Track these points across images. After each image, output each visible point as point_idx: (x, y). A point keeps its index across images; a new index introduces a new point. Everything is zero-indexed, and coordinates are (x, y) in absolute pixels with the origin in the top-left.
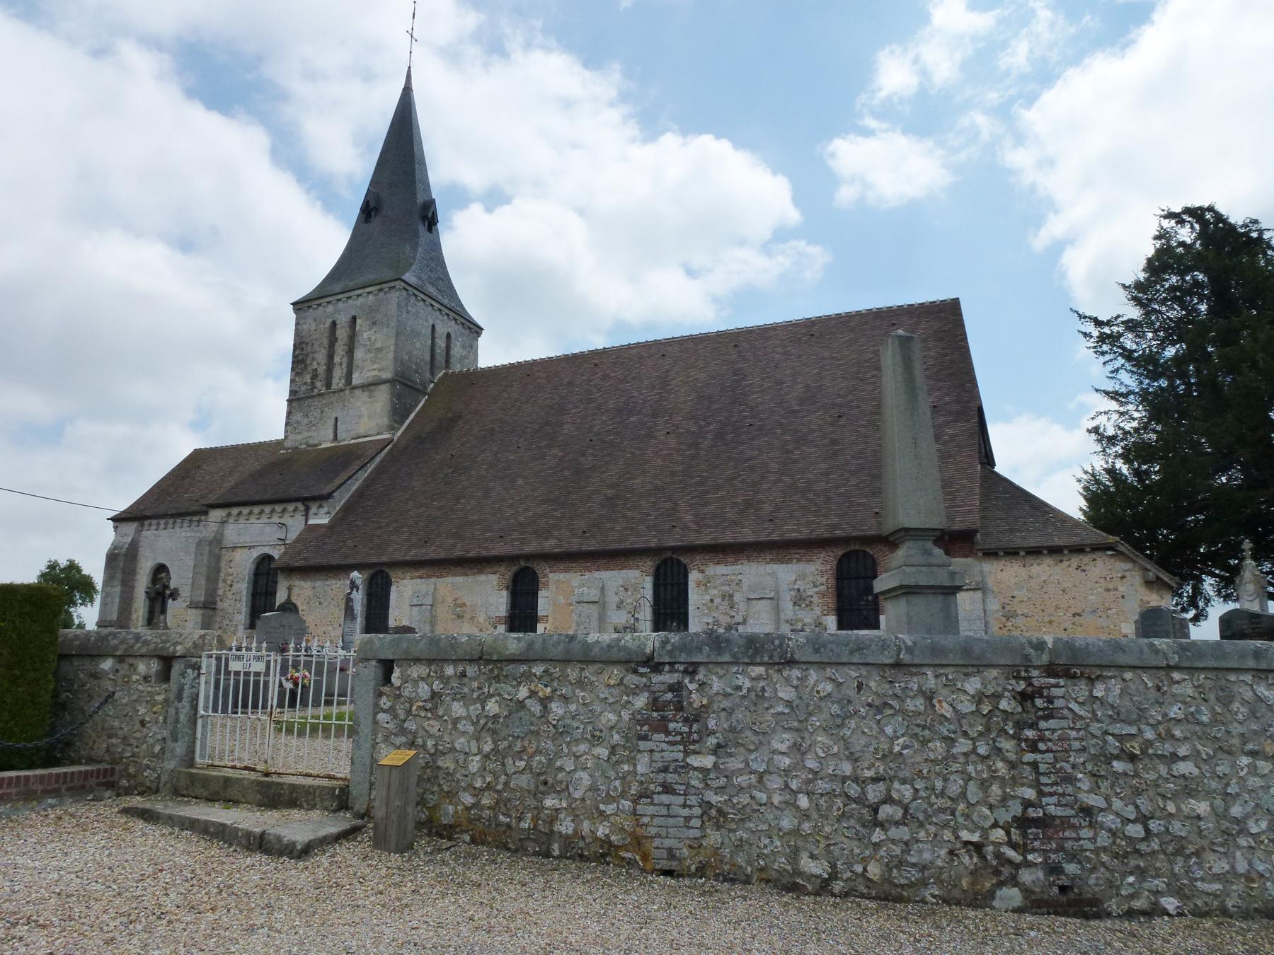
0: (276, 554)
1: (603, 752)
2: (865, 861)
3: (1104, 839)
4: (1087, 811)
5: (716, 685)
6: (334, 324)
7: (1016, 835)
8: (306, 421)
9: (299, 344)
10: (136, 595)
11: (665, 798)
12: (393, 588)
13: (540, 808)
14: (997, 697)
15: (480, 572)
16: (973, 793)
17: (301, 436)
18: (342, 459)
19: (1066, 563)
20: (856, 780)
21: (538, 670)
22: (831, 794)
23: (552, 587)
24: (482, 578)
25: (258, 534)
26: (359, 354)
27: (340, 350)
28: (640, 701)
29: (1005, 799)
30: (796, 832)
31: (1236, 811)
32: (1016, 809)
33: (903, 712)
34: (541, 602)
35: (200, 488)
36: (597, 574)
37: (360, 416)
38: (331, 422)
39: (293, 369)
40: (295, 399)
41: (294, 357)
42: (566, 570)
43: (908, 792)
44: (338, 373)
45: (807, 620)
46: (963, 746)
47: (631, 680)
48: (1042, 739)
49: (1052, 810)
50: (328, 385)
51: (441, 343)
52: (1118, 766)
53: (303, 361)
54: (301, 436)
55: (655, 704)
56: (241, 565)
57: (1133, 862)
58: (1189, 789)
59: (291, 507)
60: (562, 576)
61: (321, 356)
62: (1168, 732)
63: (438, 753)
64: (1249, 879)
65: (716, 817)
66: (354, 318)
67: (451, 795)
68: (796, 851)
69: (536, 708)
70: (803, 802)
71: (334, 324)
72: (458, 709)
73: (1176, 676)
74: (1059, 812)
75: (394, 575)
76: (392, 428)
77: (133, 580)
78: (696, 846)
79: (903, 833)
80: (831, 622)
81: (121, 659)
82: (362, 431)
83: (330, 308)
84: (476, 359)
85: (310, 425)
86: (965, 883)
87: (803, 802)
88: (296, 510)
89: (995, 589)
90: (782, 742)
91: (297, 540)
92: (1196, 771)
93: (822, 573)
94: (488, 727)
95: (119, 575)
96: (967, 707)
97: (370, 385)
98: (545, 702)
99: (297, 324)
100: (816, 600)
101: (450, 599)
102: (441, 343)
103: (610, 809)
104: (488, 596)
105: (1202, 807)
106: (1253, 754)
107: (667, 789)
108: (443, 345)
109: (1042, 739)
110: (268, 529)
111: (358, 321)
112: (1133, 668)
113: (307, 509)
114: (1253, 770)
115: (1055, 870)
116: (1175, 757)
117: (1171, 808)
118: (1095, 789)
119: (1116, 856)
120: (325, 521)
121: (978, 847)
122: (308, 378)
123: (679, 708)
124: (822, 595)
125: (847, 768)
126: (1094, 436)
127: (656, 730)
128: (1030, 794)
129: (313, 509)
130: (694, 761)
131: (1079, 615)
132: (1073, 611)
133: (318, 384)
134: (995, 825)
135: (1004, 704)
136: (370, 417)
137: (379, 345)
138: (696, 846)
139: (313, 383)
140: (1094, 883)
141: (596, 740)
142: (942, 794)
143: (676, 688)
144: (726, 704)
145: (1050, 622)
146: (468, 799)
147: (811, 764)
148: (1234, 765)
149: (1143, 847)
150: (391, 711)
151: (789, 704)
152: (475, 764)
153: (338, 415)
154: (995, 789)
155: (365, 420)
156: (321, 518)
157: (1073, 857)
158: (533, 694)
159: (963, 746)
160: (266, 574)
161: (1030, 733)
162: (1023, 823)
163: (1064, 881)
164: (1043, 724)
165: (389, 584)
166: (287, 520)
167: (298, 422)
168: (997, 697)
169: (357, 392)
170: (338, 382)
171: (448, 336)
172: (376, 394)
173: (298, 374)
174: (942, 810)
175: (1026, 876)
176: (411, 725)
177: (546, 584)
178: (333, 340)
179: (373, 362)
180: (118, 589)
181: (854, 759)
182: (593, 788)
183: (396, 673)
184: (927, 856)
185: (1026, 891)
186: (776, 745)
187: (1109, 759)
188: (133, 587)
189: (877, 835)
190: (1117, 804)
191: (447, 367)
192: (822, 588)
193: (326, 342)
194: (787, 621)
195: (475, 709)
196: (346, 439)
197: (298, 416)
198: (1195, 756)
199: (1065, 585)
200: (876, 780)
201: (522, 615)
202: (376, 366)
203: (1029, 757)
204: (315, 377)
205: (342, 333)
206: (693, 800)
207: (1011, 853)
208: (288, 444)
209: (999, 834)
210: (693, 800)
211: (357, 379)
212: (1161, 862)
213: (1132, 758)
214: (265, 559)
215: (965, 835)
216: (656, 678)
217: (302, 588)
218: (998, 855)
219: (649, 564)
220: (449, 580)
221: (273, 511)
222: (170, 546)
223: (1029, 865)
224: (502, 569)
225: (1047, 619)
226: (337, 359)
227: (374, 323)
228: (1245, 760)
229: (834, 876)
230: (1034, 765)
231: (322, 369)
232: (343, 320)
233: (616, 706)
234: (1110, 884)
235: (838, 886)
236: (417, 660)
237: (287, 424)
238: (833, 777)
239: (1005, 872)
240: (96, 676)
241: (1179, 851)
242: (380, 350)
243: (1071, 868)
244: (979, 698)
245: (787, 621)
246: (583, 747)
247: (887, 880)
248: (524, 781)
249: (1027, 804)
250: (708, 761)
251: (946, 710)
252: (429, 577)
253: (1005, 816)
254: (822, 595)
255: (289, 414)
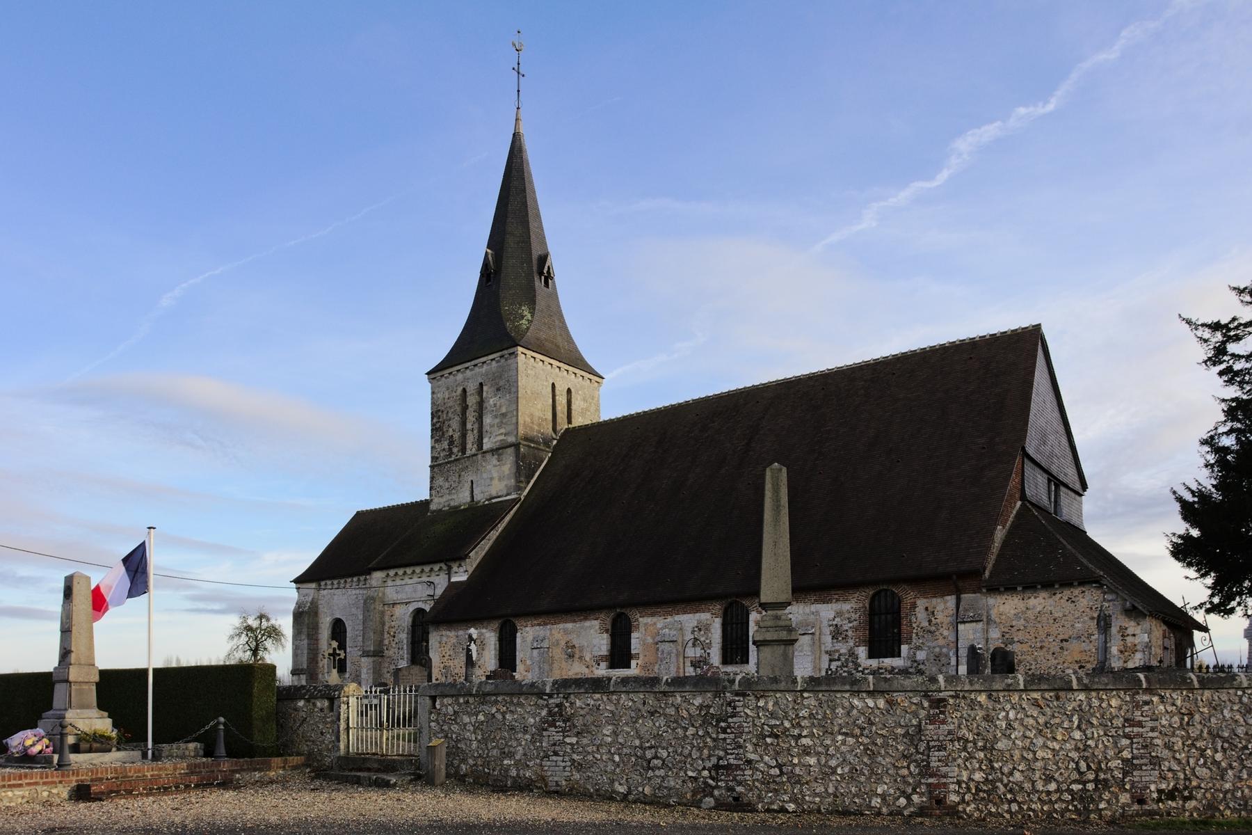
0: (427, 608)
1: (528, 737)
2: (644, 786)
3: (759, 775)
4: (749, 762)
5: (578, 703)
6: (464, 391)
7: (713, 773)
8: (447, 485)
9: (438, 416)
10: (320, 636)
11: (554, 758)
12: (518, 635)
13: (502, 765)
14: (709, 707)
15: (586, 619)
16: (695, 754)
17: (445, 499)
18: (478, 517)
19: (1059, 596)
20: (641, 748)
21: (500, 699)
22: (630, 755)
23: (642, 629)
24: (587, 624)
25: (411, 590)
26: (487, 420)
27: (471, 416)
28: (544, 713)
29: (710, 756)
30: (613, 772)
31: (833, 763)
32: (714, 760)
33: (665, 715)
34: (633, 641)
35: (367, 546)
36: (677, 618)
37: (492, 479)
38: (468, 485)
39: (432, 437)
40: (437, 466)
41: (433, 425)
42: (652, 615)
43: (665, 755)
44: (471, 438)
45: (843, 651)
46: (691, 731)
47: (541, 702)
48: (729, 727)
49: (732, 761)
50: (463, 450)
51: (562, 400)
52: (769, 740)
53: (440, 429)
54: (445, 499)
55: (550, 713)
56: (403, 616)
57: (772, 786)
58: (806, 751)
59: (436, 567)
60: (649, 620)
61: (455, 424)
62: (798, 724)
63: (458, 741)
64: (835, 796)
65: (579, 766)
66: (481, 384)
67: (464, 761)
68: (613, 781)
69: (499, 716)
70: (617, 758)
71: (464, 391)
72: (466, 719)
73: (806, 695)
74: (735, 762)
75: (519, 624)
76: (519, 489)
77: (317, 633)
78: (568, 780)
79: (662, 773)
80: (862, 652)
81: (308, 701)
82: (494, 494)
83: (460, 377)
84: (598, 410)
85: (450, 489)
86: (688, 796)
87: (617, 758)
88: (441, 569)
89: (998, 620)
90: (607, 730)
91: (442, 596)
92: (811, 743)
93: (856, 611)
94: (477, 727)
95: (305, 630)
96: (693, 711)
97: (498, 449)
98: (504, 714)
99: (433, 393)
100: (850, 633)
101: (563, 643)
102: (562, 400)
103: (531, 764)
104: (592, 637)
105: (812, 761)
106: (846, 734)
107: (556, 754)
108: (565, 402)
109: (729, 727)
110: (420, 586)
111: (485, 388)
112: (781, 691)
113: (450, 568)
114: (844, 742)
115: (731, 789)
116: (800, 736)
117: (796, 761)
118: (755, 751)
119: (763, 783)
120: (464, 578)
121: (695, 779)
122: (445, 445)
123: (561, 715)
124: (856, 629)
125: (637, 742)
126: (1207, 448)
127: (550, 726)
128: (721, 753)
129: (455, 568)
130: (568, 740)
131: (1066, 641)
132: (1061, 637)
133: (455, 450)
134: (704, 768)
135: (712, 711)
136: (500, 480)
137: (504, 410)
138: (568, 780)
139: (450, 449)
140: (751, 796)
141: (525, 732)
142: (681, 754)
143: (560, 705)
144: (582, 712)
145: (1041, 648)
146: (471, 762)
147: (621, 740)
148: (834, 740)
149: (778, 779)
150: (436, 721)
151: (612, 712)
152: (475, 745)
153: (474, 478)
154: (706, 752)
155: (496, 482)
156: (460, 576)
157: (740, 783)
158: (498, 710)
159: (691, 731)
160: (422, 625)
161: (723, 724)
162: (717, 767)
163: (735, 795)
164: (730, 720)
165: (516, 631)
166: (433, 578)
167: (441, 487)
168: (709, 707)
169: (488, 456)
170: (471, 448)
171: (569, 391)
172: (504, 457)
173: (436, 441)
174: (680, 762)
175: (716, 793)
176: (445, 728)
177: (637, 627)
178: (465, 408)
179: (500, 427)
180: (306, 642)
181: (640, 738)
182: (525, 755)
183: (438, 702)
184: (672, 783)
185: (716, 800)
186: (605, 732)
187: (764, 737)
188: (317, 640)
189: (650, 773)
190: (766, 758)
191: (570, 422)
192: (855, 623)
193: (458, 409)
194: (827, 652)
195: (473, 719)
196: (480, 497)
197: (440, 481)
198: (811, 735)
199: (1056, 615)
200: (650, 748)
201: (620, 655)
202: (503, 431)
203: (722, 736)
204: (451, 443)
205: (472, 400)
206: (567, 758)
207: (711, 782)
208: (433, 507)
209: (706, 773)
210: (567, 758)
211: (487, 444)
212: (788, 787)
213: (777, 736)
214: (419, 612)
215: (690, 774)
216: (551, 701)
217: (448, 637)
218: (705, 783)
219: (718, 607)
220: (561, 626)
221: (422, 571)
222: (340, 600)
223: (717, 787)
224: (602, 616)
225: (1039, 645)
226: (469, 426)
227: (498, 390)
228: (840, 738)
229: (629, 792)
230: (725, 739)
231: (457, 436)
232: (472, 387)
233: (534, 715)
234: (759, 797)
235: (631, 797)
236: (447, 696)
237: (431, 488)
238: (631, 747)
239: (707, 790)
240: (296, 710)
241: (798, 782)
242: (504, 415)
243: (739, 789)
244: (701, 707)
245: (827, 652)
246: (520, 735)
247: (654, 795)
248: (495, 752)
249: (720, 758)
250: (574, 740)
251: (685, 714)
252: (546, 624)
253: (709, 765)
254: (856, 629)
255: (432, 479)
